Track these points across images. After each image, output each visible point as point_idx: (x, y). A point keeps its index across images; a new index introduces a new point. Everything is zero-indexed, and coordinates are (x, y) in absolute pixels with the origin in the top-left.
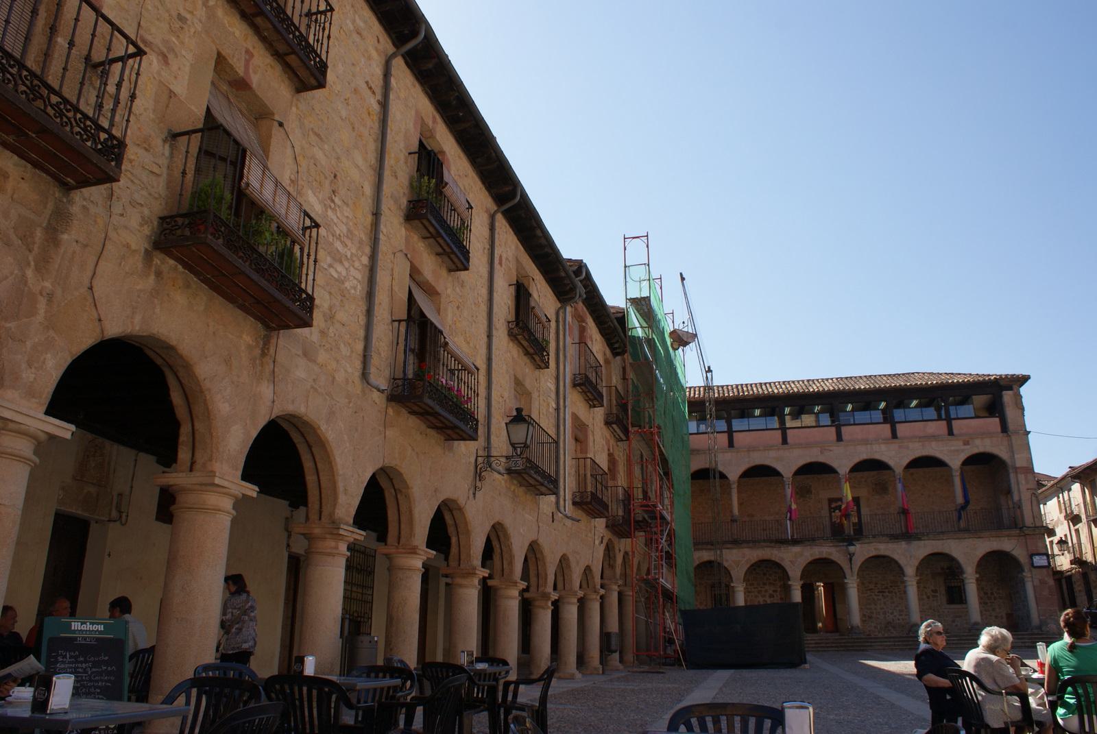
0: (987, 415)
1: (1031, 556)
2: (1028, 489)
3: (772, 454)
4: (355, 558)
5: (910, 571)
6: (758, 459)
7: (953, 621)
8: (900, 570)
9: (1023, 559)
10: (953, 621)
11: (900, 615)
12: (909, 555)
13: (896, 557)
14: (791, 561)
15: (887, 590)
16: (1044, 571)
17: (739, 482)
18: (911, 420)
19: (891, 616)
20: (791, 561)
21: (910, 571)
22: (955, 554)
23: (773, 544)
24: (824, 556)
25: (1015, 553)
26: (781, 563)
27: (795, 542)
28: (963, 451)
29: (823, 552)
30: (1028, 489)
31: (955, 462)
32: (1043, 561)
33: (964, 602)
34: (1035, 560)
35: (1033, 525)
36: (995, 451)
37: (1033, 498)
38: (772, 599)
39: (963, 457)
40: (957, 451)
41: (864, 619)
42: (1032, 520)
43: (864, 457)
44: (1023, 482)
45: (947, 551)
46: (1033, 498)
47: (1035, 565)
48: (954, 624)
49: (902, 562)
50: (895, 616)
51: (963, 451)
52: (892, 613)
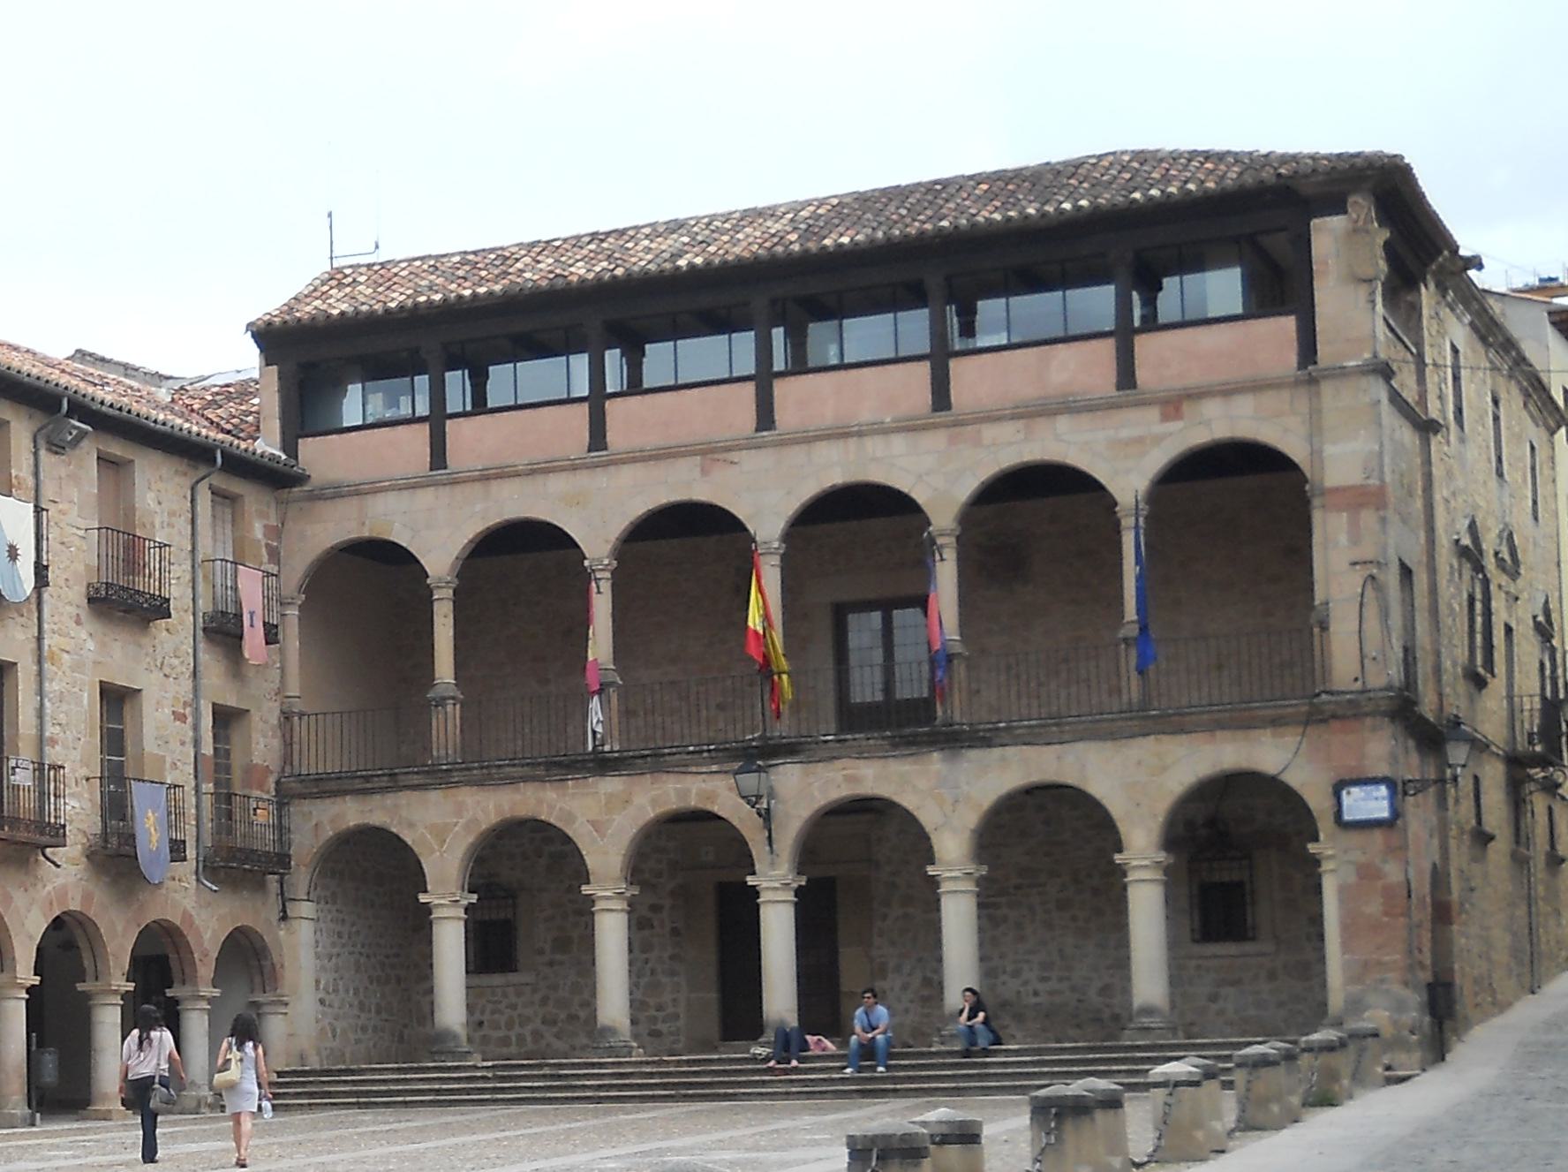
0: (1491, 301)
1: (1338, 788)
2: (1355, 564)
3: (558, 484)
4: (915, 676)
5: (952, 850)
6: (684, 484)
7: (1214, 998)
8: (919, 844)
9: (1317, 799)
10: (1214, 998)
11: (1044, 979)
12: (949, 798)
13: (908, 801)
14: (593, 823)
15: (1003, 900)
16: (1378, 836)
17: (789, 535)
18: (1094, 343)
19: (1014, 984)
20: (593, 823)
21: (952, 850)
22: (1099, 788)
23: (540, 772)
24: (693, 802)
25: (1293, 779)
26: (709, 807)
27: (603, 764)
28: (1158, 440)
29: (689, 791)
30: (1355, 564)
31: (1128, 481)
32: (1373, 804)
33: (1250, 934)
34: (1346, 800)
35: (1358, 686)
36: (1268, 434)
37: (1369, 593)
38: (646, 933)
39: (1158, 459)
40: (1140, 440)
41: (926, 992)
42: (1354, 669)
43: (837, 477)
44: (1343, 539)
45: (1070, 779)
46: (1369, 593)
47: (1347, 817)
48: (1214, 1007)
49: (928, 817)
50: (1026, 983)
51: (1158, 440)
52: (1016, 974)
